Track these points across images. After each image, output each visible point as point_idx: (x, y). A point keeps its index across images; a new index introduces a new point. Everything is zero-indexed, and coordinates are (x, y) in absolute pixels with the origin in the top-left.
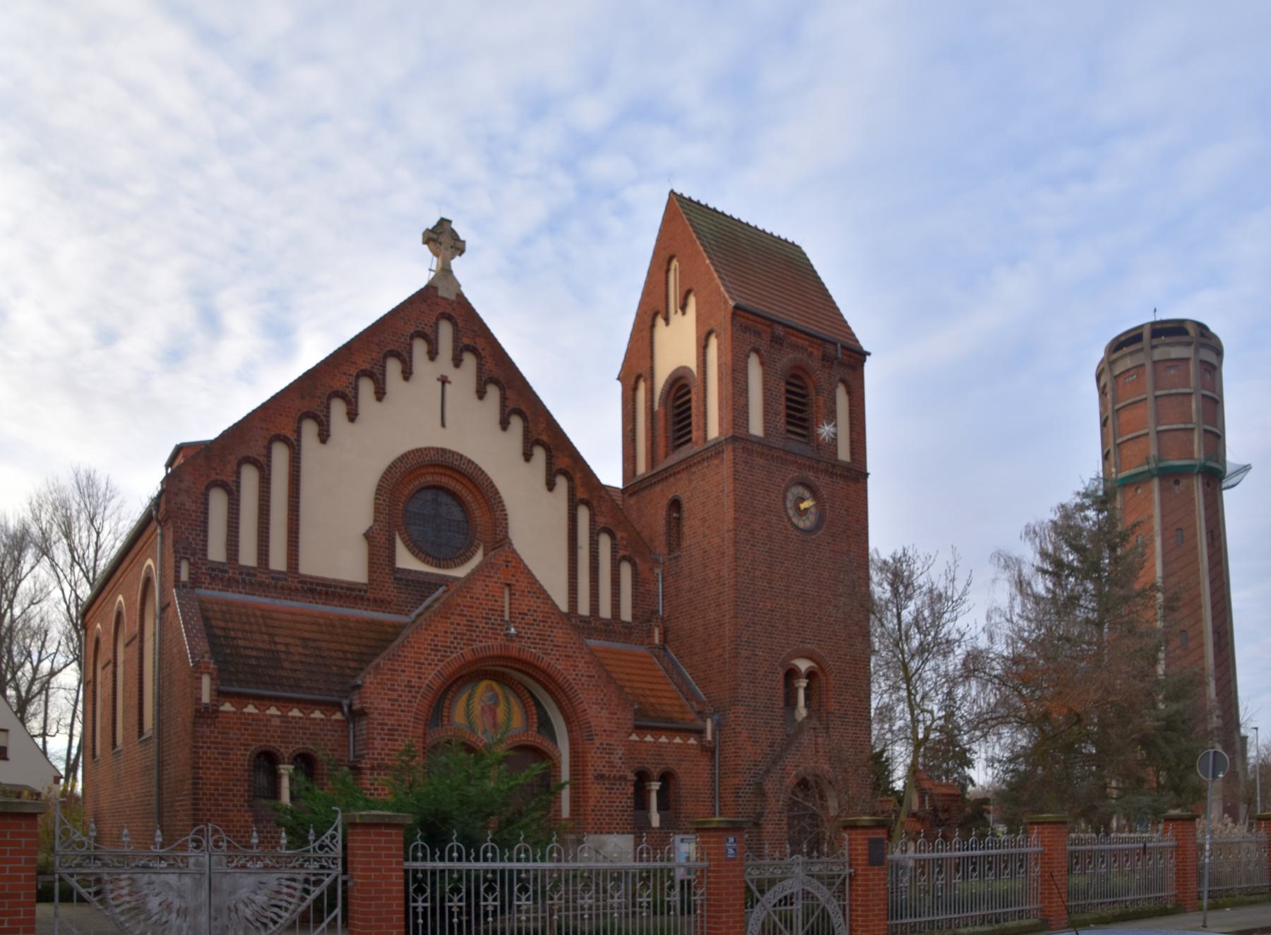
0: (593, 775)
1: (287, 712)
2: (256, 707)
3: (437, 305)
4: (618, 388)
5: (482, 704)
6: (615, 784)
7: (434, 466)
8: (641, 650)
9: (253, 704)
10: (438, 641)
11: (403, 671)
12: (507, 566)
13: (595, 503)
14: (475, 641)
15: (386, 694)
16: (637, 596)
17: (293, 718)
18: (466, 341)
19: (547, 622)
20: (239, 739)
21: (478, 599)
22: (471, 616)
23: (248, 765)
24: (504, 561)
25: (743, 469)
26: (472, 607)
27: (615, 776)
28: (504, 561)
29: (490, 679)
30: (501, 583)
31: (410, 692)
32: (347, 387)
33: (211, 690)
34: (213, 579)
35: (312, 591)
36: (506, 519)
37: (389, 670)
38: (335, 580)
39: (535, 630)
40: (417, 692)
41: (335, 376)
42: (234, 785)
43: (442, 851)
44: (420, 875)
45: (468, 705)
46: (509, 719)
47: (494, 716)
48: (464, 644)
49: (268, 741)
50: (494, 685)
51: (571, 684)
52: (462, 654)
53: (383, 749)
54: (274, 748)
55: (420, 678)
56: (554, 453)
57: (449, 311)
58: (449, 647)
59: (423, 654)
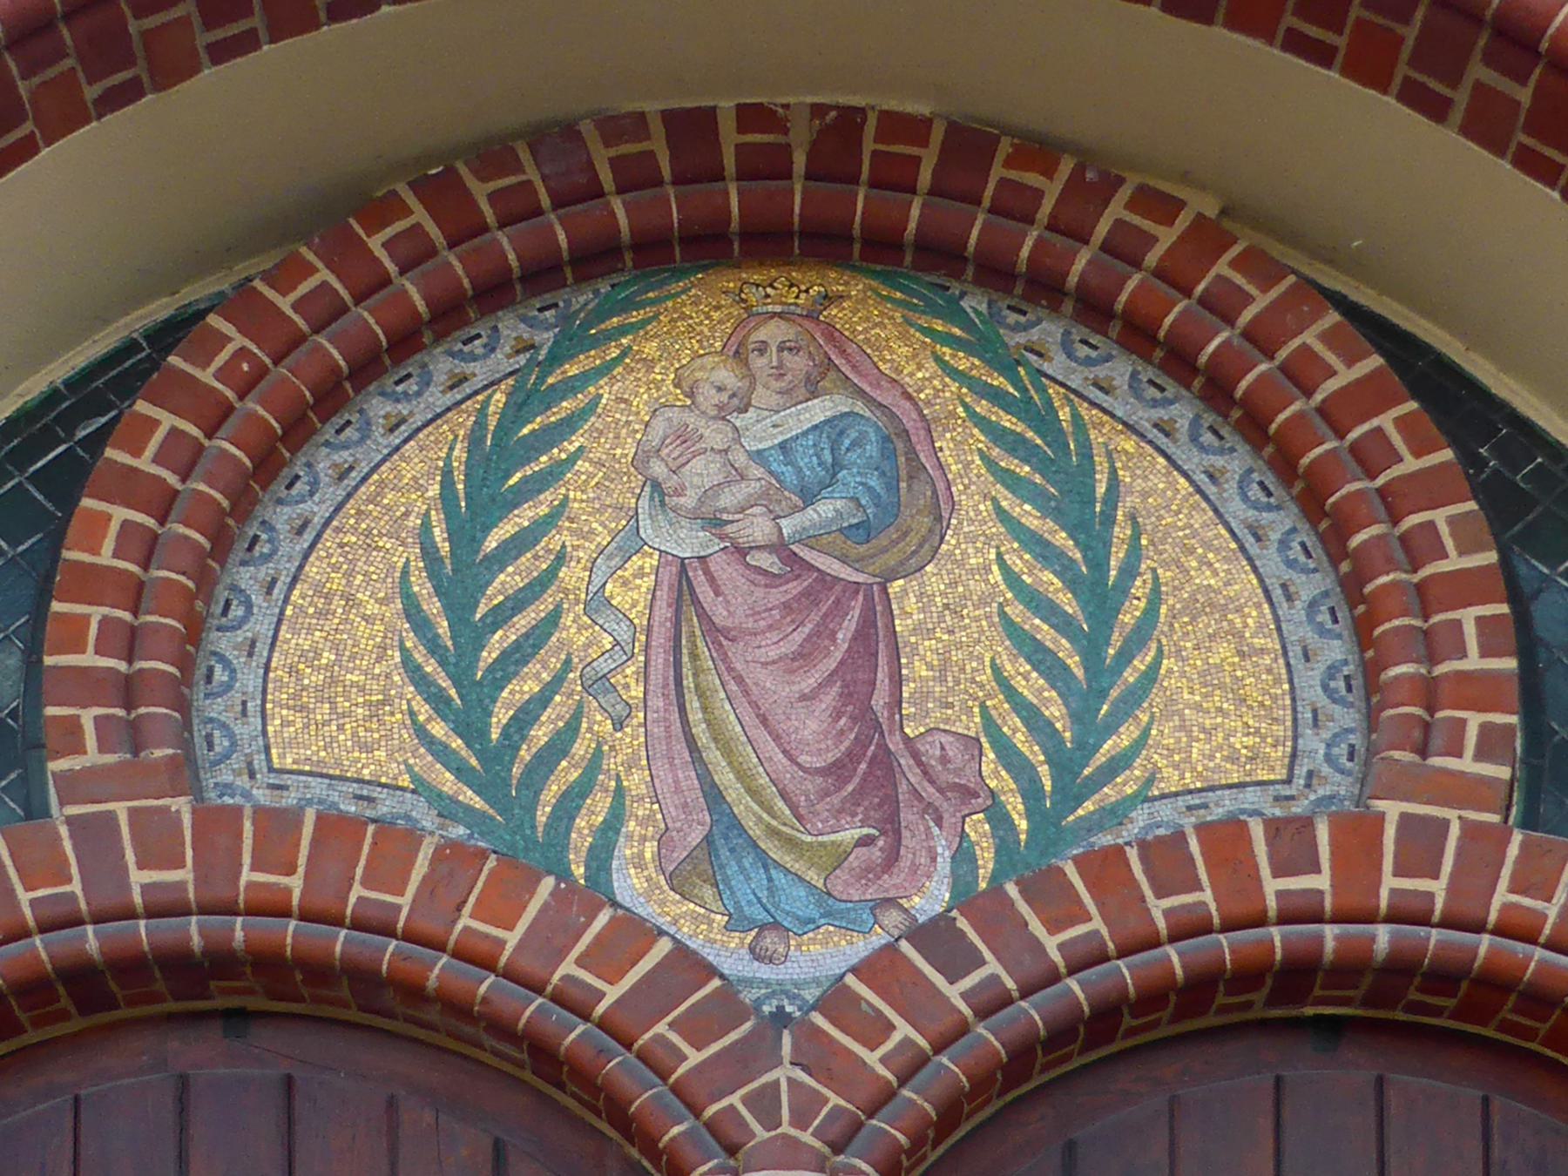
5: (690, 542)
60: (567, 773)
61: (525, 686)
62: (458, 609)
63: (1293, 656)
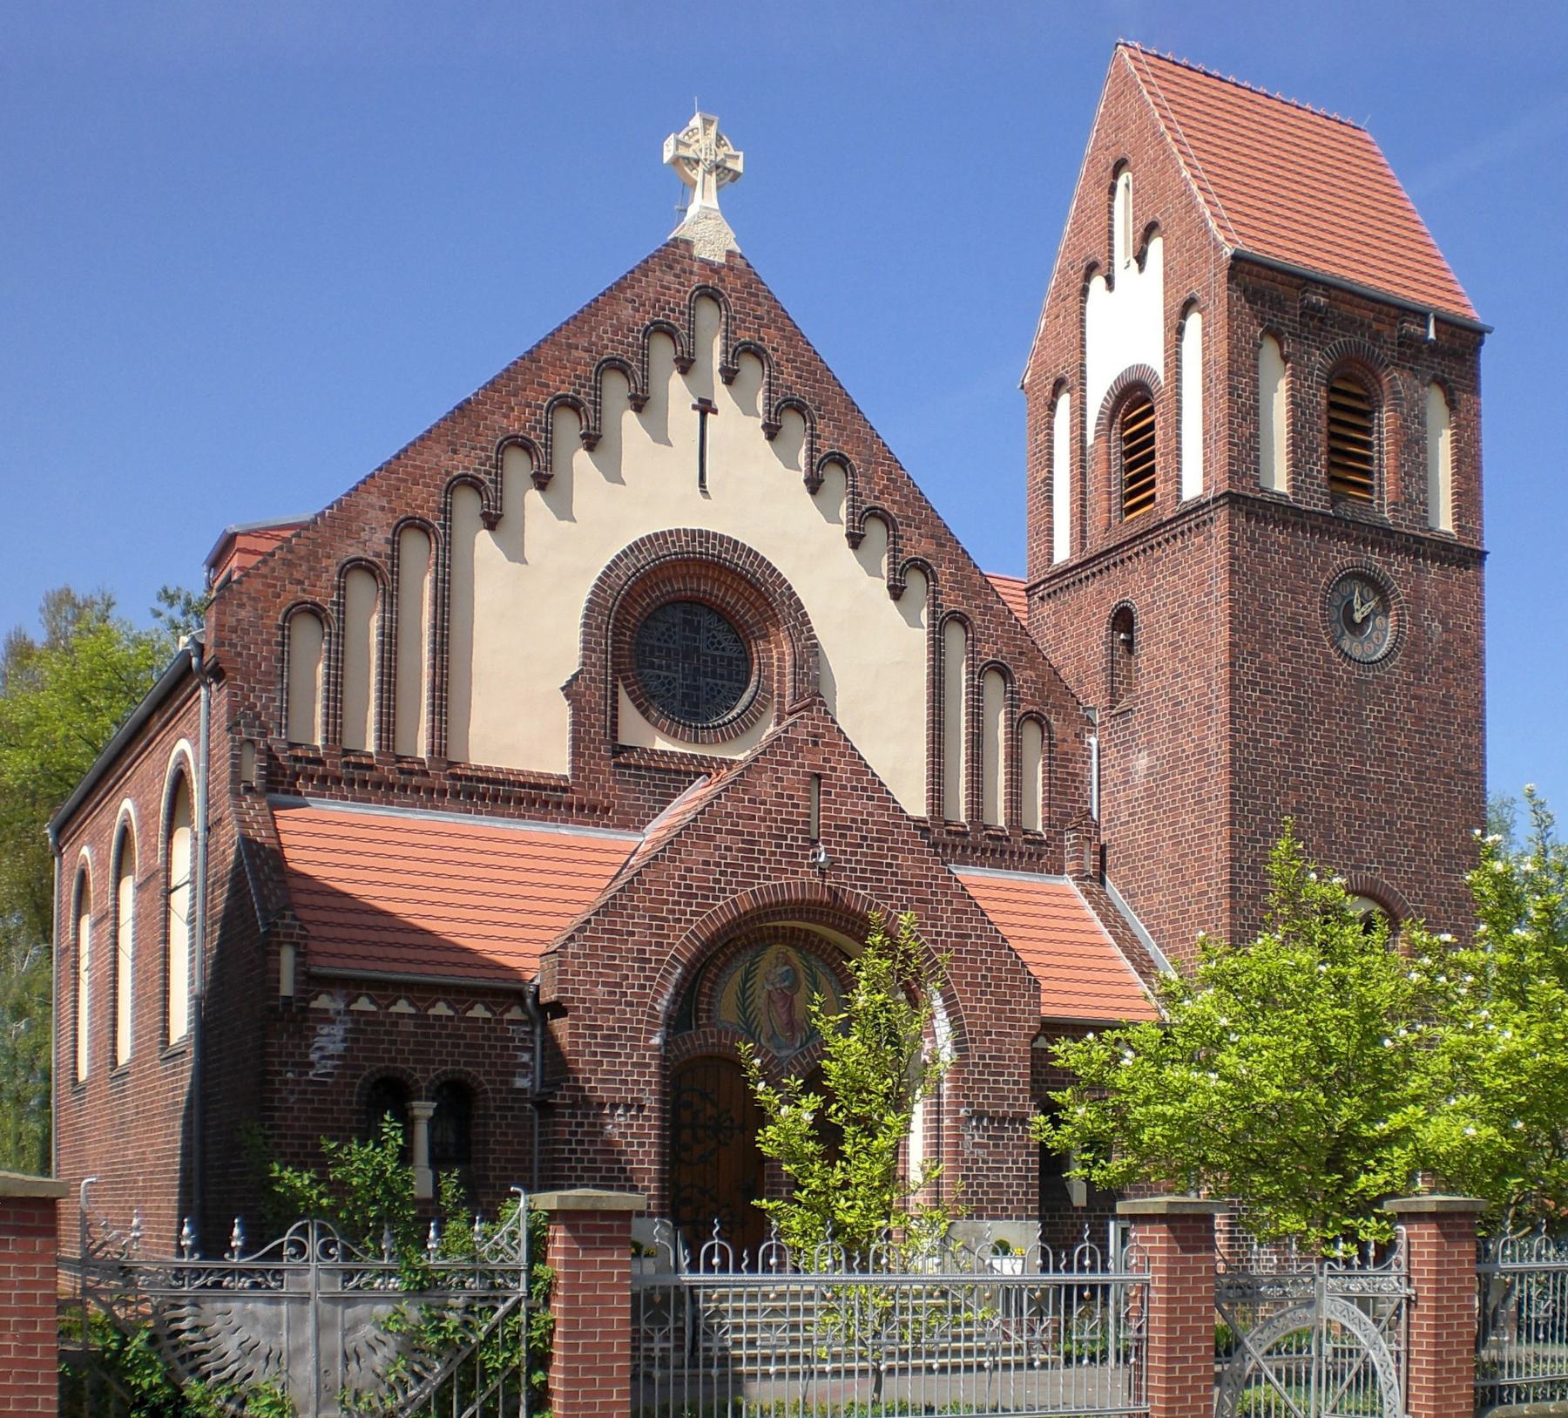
1: (427, 1009)
2: (373, 1002)
11: (632, 934)
12: (815, 744)
14: (758, 877)
18: (745, 337)
22: (750, 834)
26: (753, 818)
31: (643, 969)
40: (657, 970)
43: (864, 1258)
48: (738, 883)
49: (394, 1060)
50: (791, 953)
62: (743, 995)
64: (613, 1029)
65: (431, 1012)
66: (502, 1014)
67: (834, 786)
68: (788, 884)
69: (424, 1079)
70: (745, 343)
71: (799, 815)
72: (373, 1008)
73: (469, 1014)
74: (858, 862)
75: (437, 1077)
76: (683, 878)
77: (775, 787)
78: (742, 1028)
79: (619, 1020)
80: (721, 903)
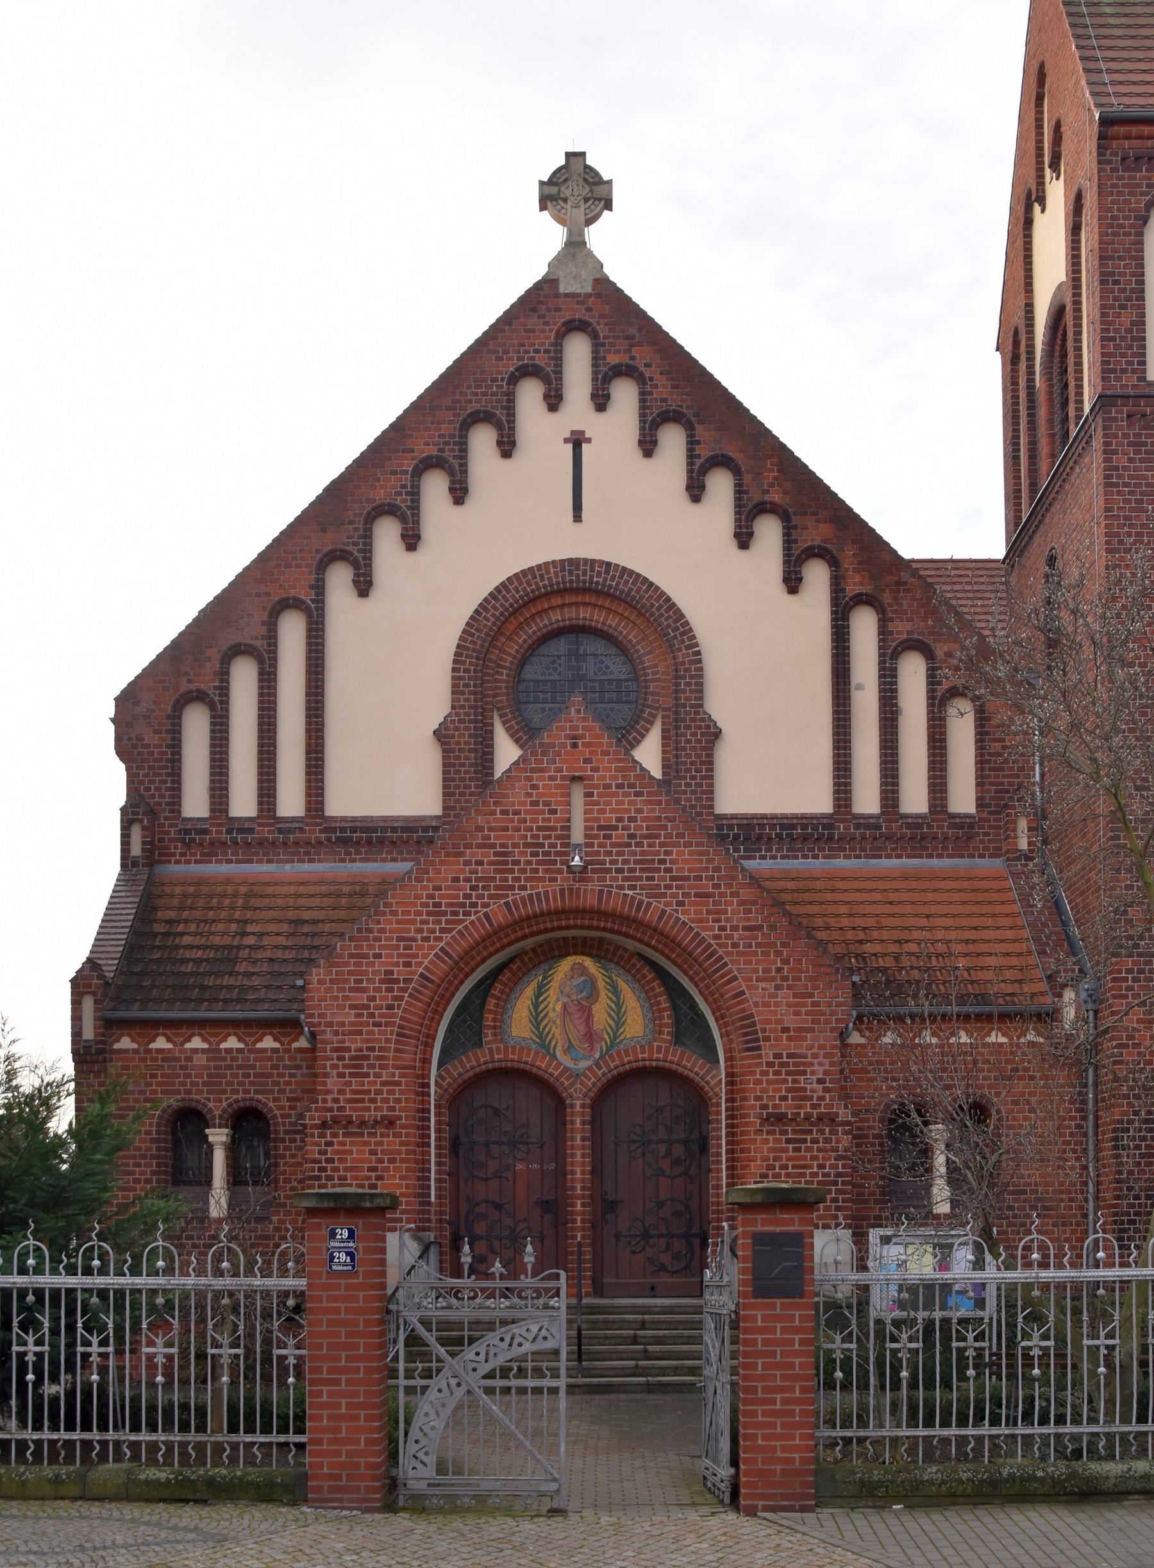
0: (760, 1116)
1: (219, 1043)
2: (169, 1040)
3: (558, 310)
4: (996, 360)
5: (566, 1000)
6: (810, 1132)
7: (561, 592)
8: (995, 864)
9: (164, 1035)
10: (440, 896)
11: (379, 956)
12: (575, 745)
13: (887, 598)
14: (512, 888)
15: (347, 998)
16: (172, 761)
17: (229, 1051)
18: (613, 359)
19: (658, 836)
20: (142, 1092)
21: (516, 813)
22: (503, 845)
23: (158, 1132)
24: (567, 737)
25: (1131, 460)
26: (506, 829)
27: (808, 1117)
28: (567, 737)
29: (576, 953)
30: (563, 778)
31: (391, 990)
32: (400, 494)
33: (95, 1019)
34: (187, 845)
35: (345, 842)
36: (700, 661)
37: (351, 956)
38: (384, 819)
39: (634, 853)
40: (405, 990)
41: (378, 480)
42: (136, 1165)
43: (137, 1258)
44: (31, 1298)
45: (536, 1005)
46: (619, 1022)
47: (589, 1018)
48: (490, 897)
49: (189, 1092)
50: (588, 962)
51: (710, 945)
52: (486, 915)
53: (340, 1092)
54: (198, 1101)
55: (408, 964)
56: (795, 520)
57: (580, 314)
58: (463, 905)
59: (413, 922)
60: (550, 1036)
61: (544, 1023)
62: (536, 1010)
63: (644, 1016)
64: (361, 1050)
65: (223, 1046)
66: (290, 1043)
67: (597, 786)
68: (546, 893)
69: (217, 1108)
70: (614, 367)
71: (557, 820)
72: (170, 1046)
73: (259, 1045)
74: (625, 862)
75: (230, 1105)
76: (432, 897)
77: (529, 795)
78: (535, 1043)
79: (367, 1041)
80: (473, 917)
